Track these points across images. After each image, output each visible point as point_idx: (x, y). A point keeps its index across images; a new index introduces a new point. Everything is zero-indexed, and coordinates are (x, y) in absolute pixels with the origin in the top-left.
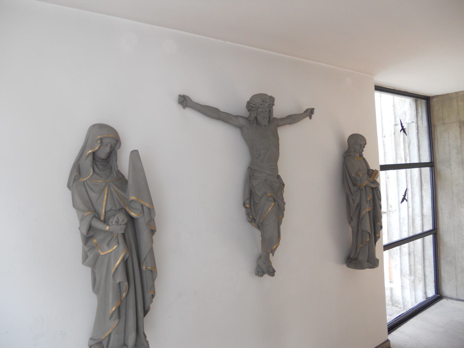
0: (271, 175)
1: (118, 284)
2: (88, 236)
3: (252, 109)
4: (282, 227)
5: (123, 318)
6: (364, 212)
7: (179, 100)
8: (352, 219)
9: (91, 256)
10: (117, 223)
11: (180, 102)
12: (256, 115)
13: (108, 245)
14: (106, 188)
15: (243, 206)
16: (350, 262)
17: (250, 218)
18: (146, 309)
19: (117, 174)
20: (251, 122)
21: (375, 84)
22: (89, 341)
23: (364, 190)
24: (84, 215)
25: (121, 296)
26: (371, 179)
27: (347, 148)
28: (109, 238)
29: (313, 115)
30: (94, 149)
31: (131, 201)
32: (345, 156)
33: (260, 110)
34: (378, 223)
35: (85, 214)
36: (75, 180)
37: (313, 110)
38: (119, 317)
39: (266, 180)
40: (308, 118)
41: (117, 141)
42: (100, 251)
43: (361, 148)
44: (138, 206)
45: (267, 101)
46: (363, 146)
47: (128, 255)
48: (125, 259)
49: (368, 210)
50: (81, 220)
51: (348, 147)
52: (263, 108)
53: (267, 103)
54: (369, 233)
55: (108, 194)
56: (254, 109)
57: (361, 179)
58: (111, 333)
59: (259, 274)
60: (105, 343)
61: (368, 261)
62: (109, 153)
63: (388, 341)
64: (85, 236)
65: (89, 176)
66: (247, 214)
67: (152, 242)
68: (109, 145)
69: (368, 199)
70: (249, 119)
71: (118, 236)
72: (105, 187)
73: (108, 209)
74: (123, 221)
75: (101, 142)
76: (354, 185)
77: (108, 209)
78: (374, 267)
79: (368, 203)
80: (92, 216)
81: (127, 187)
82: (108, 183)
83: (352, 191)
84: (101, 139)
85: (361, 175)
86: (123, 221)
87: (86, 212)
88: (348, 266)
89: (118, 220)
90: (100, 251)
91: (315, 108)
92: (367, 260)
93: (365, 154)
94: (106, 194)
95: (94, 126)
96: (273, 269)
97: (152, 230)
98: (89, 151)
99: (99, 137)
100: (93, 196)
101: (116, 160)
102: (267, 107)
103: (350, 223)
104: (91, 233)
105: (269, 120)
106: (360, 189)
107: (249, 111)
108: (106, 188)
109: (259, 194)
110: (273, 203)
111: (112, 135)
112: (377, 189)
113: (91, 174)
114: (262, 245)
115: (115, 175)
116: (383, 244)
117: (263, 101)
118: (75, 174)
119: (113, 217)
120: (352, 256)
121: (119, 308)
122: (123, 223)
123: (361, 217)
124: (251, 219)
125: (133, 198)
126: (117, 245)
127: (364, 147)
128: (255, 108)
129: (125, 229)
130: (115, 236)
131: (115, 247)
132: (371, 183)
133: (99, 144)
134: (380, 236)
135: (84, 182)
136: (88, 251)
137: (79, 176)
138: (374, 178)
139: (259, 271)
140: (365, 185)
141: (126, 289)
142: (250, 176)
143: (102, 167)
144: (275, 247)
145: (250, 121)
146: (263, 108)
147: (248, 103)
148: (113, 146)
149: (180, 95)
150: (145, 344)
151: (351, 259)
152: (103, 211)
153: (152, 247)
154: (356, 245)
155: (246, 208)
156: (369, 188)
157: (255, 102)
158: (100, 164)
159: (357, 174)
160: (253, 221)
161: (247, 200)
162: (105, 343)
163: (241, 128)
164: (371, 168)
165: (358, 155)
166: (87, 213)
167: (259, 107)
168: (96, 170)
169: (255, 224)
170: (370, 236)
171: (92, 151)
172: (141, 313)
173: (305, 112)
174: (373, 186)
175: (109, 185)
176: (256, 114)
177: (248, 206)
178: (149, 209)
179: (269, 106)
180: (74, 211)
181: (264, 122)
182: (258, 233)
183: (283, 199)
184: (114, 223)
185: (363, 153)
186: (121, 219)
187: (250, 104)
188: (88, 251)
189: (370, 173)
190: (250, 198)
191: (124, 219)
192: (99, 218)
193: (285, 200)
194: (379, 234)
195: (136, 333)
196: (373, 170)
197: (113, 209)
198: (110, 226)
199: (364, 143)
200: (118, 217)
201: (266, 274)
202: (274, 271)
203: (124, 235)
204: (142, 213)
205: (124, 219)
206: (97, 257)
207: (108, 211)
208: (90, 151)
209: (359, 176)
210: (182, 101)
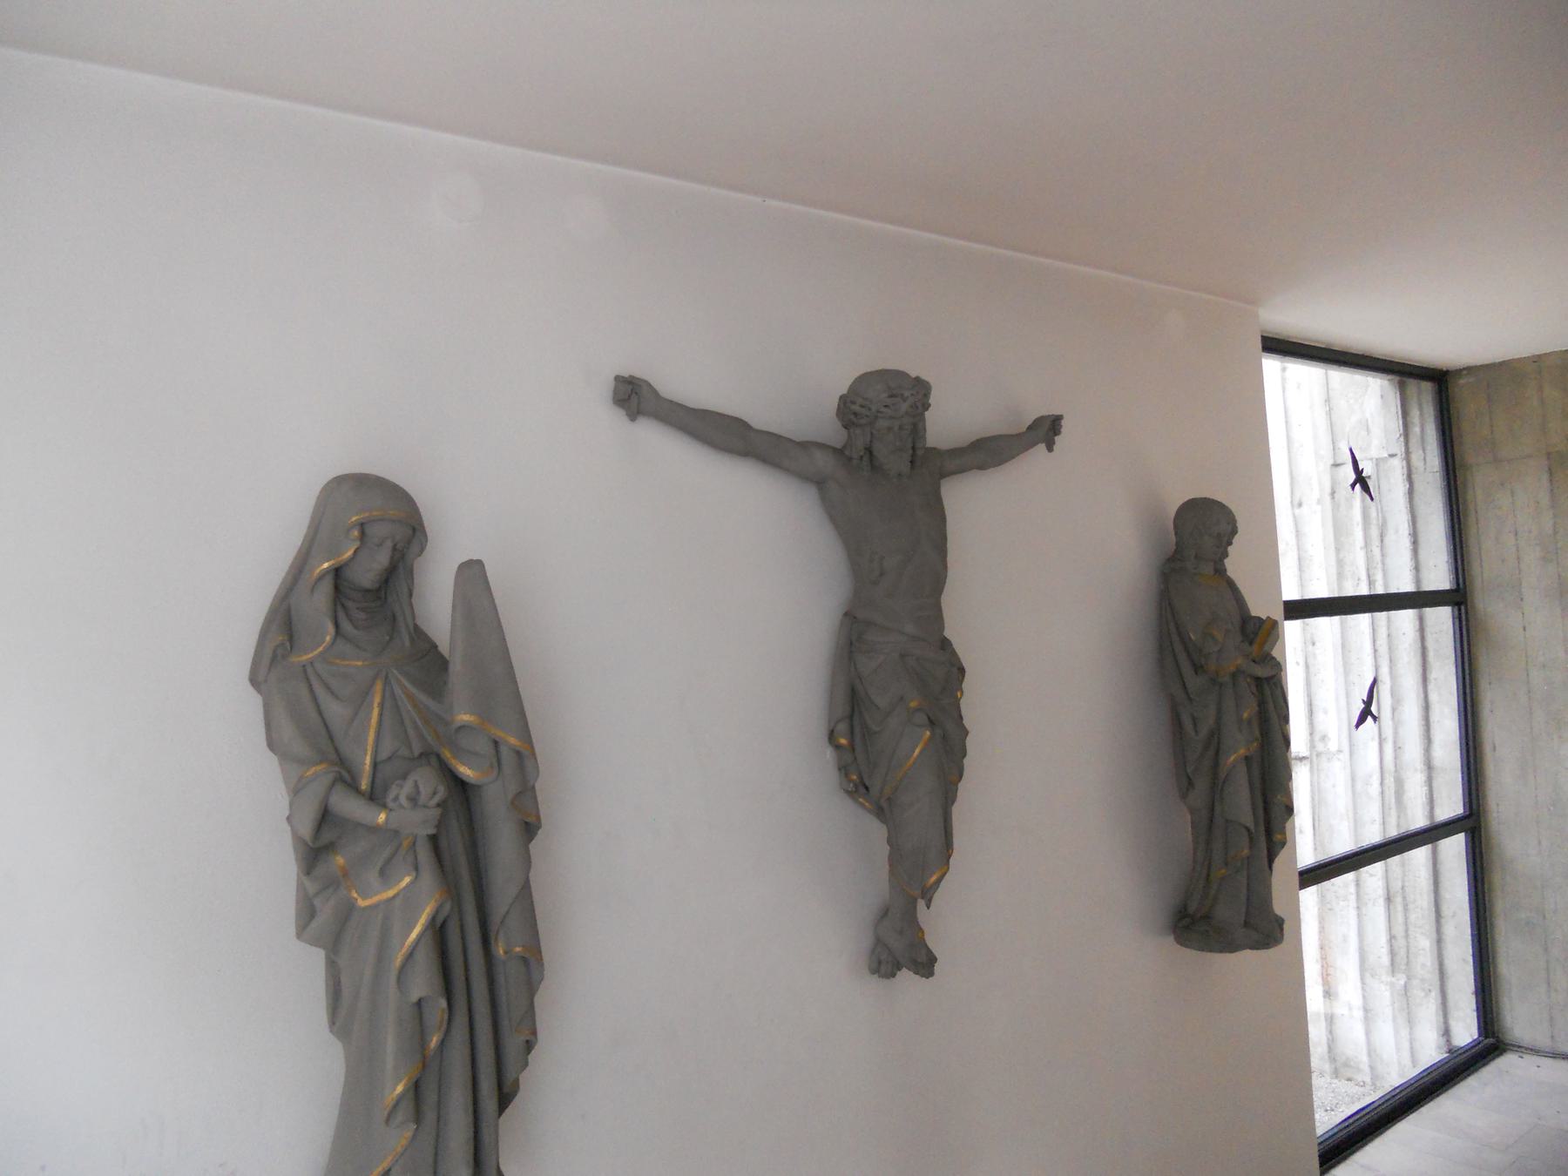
3: (855, 420)
4: (957, 811)
5: (430, 1117)
6: (1232, 758)
8: (1190, 784)
10: (413, 800)
12: (868, 439)
13: (382, 873)
14: (379, 687)
16: (1187, 928)
17: (850, 781)
18: (506, 1090)
19: (412, 640)
25: (423, 1043)
28: (386, 853)
29: (1056, 438)
30: (340, 559)
33: (882, 423)
38: (418, 1117)
39: (902, 656)
42: (355, 895)
44: (483, 746)
45: (907, 394)
48: (440, 919)
49: (1242, 751)
52: (892, 418)
53: (905, 401)
54: (1248, 830)
55: (382, 705)
56: (863, 421)
61: (1246, 924)
66: (840, 769)
67: (527, 862)
68: (389, 544)
69: (1245, 715)
70: (847, 453)
71: (414, 844)
72: (372, 685)
73: (384, 755)
74: (435, 793)
75: (363, 534)
76: (1198, 669)
78: (1268, 944)
80: (331, 777)
85: (1219, 636)
89: (418, 792)
90: (355, 895)
91: (1065, 416)
92: (1242, 922)
93: (1237, 564)
94: (376, 705)
96: (929, 951)
97: (527, 823)
99: (354, 519)
100: (336, 711)
101: (411, 595)
102: (907, 413)
104: (327, 836)
105: (914, 455)
108: (379, 687)
110: (928, 733)
112: (1275, 684)
113: (328, 638)
115: (407, 643)
117: (891, 396)
119: (398, 782)
120: (1193, 907)
123: (1222, 775)
124: (856, 786)
125: (465, 718)
126: (414, 874)
128: (867, 416)
129: (440, 822)
131: (407, 880)
133: (354, 540)
135: (304, 666)
137: (288, 644)
140: (1232, 669)
141: (441, 1022)
144: (934, 879)
145: (850, 459)
146: (892, 418)
147: (844, 400)
152: (368, 760)
153: (527, 882)
155: (837, 747)
156: (1248, 680)
163: (820, 482)
164: (1253, 614)
166: (314, 768)
167: (879, 415)
168: (346, 626)
170: (1251, 839)
172: (489, 1103)
173: (1030, 428)
174: (1261, 672)
177: (843, 741)
178: (518, 753)
180: (271, 762)
183: (961, 718)
184: (403, 800)
185: (1227, 562)
186: (425, 790)
188: (317, 894)
192: (352, 785)
196: (1259, 618)
198: (391, 810)
200: (416, 782)
201: (904, 970)
203: (434, 840)
208: (326, 565)
210: (627, 397)
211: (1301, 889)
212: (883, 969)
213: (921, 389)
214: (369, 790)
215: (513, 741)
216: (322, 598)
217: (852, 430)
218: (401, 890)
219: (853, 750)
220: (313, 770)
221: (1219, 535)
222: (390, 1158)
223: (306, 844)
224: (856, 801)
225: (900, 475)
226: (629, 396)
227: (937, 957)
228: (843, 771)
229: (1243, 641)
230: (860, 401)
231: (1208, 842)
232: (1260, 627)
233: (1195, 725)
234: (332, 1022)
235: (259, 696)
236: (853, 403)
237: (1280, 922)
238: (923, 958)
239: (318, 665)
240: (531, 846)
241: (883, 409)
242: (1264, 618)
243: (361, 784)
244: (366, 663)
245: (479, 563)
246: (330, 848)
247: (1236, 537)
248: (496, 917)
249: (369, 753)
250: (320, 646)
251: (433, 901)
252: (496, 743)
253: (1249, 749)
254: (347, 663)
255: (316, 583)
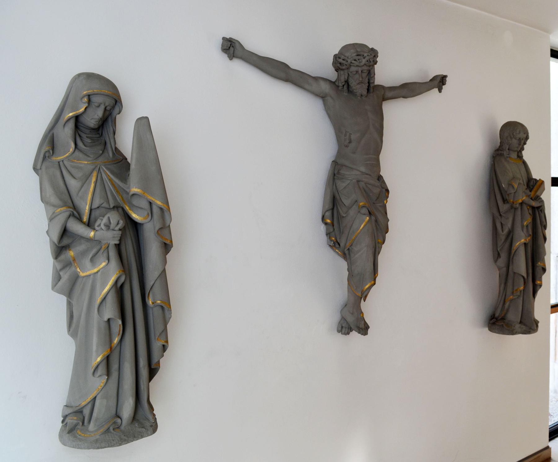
0: (367, 174)
1: (105, 321)
2: (60, 245)
3: (340, 67)
4: (381, 258)
5: (115, 374)
6: (518, 244)
7: (223, 45)
8: (499, 255)
9: (65, 276)
10: (108, 226)
11: (224, 49)
12: (346, 78)
13: (92, 260)
14: (95, 174)
15: (321, 220)
16: (494, 324)
17: (331, 240)
18: (153, 367)
19: (113, 154)
20: (340, 88)
21: (551, 47)
22: (63, 410)
23: (519, 210)
24: (56, 212)
25: (111, 341)
26: (532, 194)
27: (499, 144)
29: (443, 87)
30: (77, 112)
31: (133, 195)
32: (494, 155)
33: (353, 69)
34: (539, 263)
35: (58, 211)
36: (44, 158)
37: (444, 78)
38: (108, 373)
39: (358, 181)
40: (437, 89)
41: (116, 101)
42: (79, 270)
43: (520, 145)
45: (365, 55)
46: (523, 142)
47: (123, 279)
48: (119, 284)
49: (523, 241)
50: (51, 219)
51: (501, 143)
52: (357, 66)
53: (364, 58)
54: (523, 277)
55: (96, 183)
56: (344, 67)
57: (515, 192)
58: (96, 397)
59: (343, 331)
60: (86, 412)
61: (521, 322)
62: (101, 119)
63: (548, 448)
64: (56, 245)
65: (68, 154)
66: (327, 235)
67: (165, 262)
68: (102, 107)
69: (525, 224)
70: (337, 83)
71: (108, 247)
72: (92, 172)
73: (95, 205)
74: (118, 224)
75: (89, 101)
76: (505, 201)
77: (96, 205)
78: (530, 332)
79: (525, 230)
80: (67, 214)
81: (129, 175)
82: (98, 166)
83: (501, 210)
84: (89, 95)
85: (516, 186)
86: (118, 224)
87: (59, 208)
88: (491, 330)
89: (110, 223)
90: (79, 270)
91: (448, 76)
92: (519, 321)
93: (528, 154)
94: (93, 182)
95: (79, 75)
96: (365, 323)
97: (165, 244)
98: (69, 114)
99: (85, 93)
100: (73, 184)
101: (114, 133)
102: (365, 64)
103: (496, 261)
104: (65, 241)
105: (369, 86)
106: (513, 208)
107: (337, 70)
108: (95, 174)
109: (347, 202)
110: (368, 218)
111: (106, 91)
112: (541, 211)
113: (71, 150)
114: (349, 284)
115: (111, 155)
116: (550, 302)
117: (358, 55)
118: (46, 148)
119: (101, 218)
120: (497, 315)
121: (108, 359)
122: (117, 228)
123: (513, 252)
124: (334, 243)
125: (135, 190)
126: (107, 261)
127: (525, 144)
128: (346, 65)
129: (121, 238)
130: (103, 247)
131: (104, 264)
132: (531, 199)
133: (85, 103)
134: (542, 283)
135: (59, 162)
136: (61, 270)
137: (51, 152)
138: (536, 191)
139: (343, 325)
140: (520, 201)
141: (120, 331)
142: (334, 175)
143: (90, 141)
144: (367, 286)
145: (338, 86)
146: (357, 66)
147: (336, 57)
148: (108, 108)
149: (224, 38)
150: (150, 417)
151: (496, 319)
152: (87, 208)
153: (164, 270)
154: (503, 299)
155: (326, 224)
156: (528, 207)
157: (345, 56)
158: (88, 135)
159: (510, 185)
160: (337, 246)
161: (327, 211)
162: (86, 412)
163: (323, 97)
164: (534, 177)
165: (514, 155)
166: (60, 209)
167: (351, 64)
168: (80, 144)
169: (340, 251)
170: (525, 283)
171: (74, 113)
172: (144, 372)
173: (431, 80)
174: (535, 204)
175: (99, 169)
176: (347, 75)
177: (329, 221)
178: (161, 209)
179: (367, 63)
180: (41, 206)
181: (361, 89)
182: (344, 264)
183: (386, 213)
184: (102, 226)
185: (523, 152)
186: (113, 222)
187: (338, 59)
188: (61, 270)
189: (532, 183)
190: (333, 209)
191: (118, 221)
192: (79, 219)
193: (389, 216)
194: (541, 280)
195: (134, 399)
196: (536, 180)
197: (103, 205)
198: (96, 231)
199: (525, 136)
201: (354, 331)
202: (366, 328)
203: (118, 247)
204: (150, 214)
205: (118, 221)
206: (75, 279)
207: (95, 209)
208: (71, 114)
209: (513, 187)
210: (228, 48)
211: (552, 313)
212: (344, 330)
213: (374, 53)
214: (87, 221)
215: (159, 203)
216: (69, 129)
217: (339, 72)
218: (101, 269)
219: (333, 226)
220: (59, 210)
221: (520, 139)
222: (96, 392)
223: (56, 245)
224: (333, 250)
225: (361, 95)
226: (229, 47)
227: (370, 326)
228: (328, 235)
229: (526, 189)
230: (343, 57)
231: (506, 284)
232: (536, 183)
233: (502, 227)
234: (69, 330)
235: (38, 176)
236: (340, 58)
237: (537, 323)
238: (362, 326)
239: (65, 162)
240: (167, 256)
241: (353, 62)
242: (538, 179)
243: (84, 219)
244: (89, 162)
245: (147, 118)
246: (66, 247)
247: (528, 141)
248: (148, 287)
249: (88, 204)
250: (67, 153)
251: (116, 274)
252: (150, 203)
253: (526, 240)
254: (81, 162)
255: (66, 123)
